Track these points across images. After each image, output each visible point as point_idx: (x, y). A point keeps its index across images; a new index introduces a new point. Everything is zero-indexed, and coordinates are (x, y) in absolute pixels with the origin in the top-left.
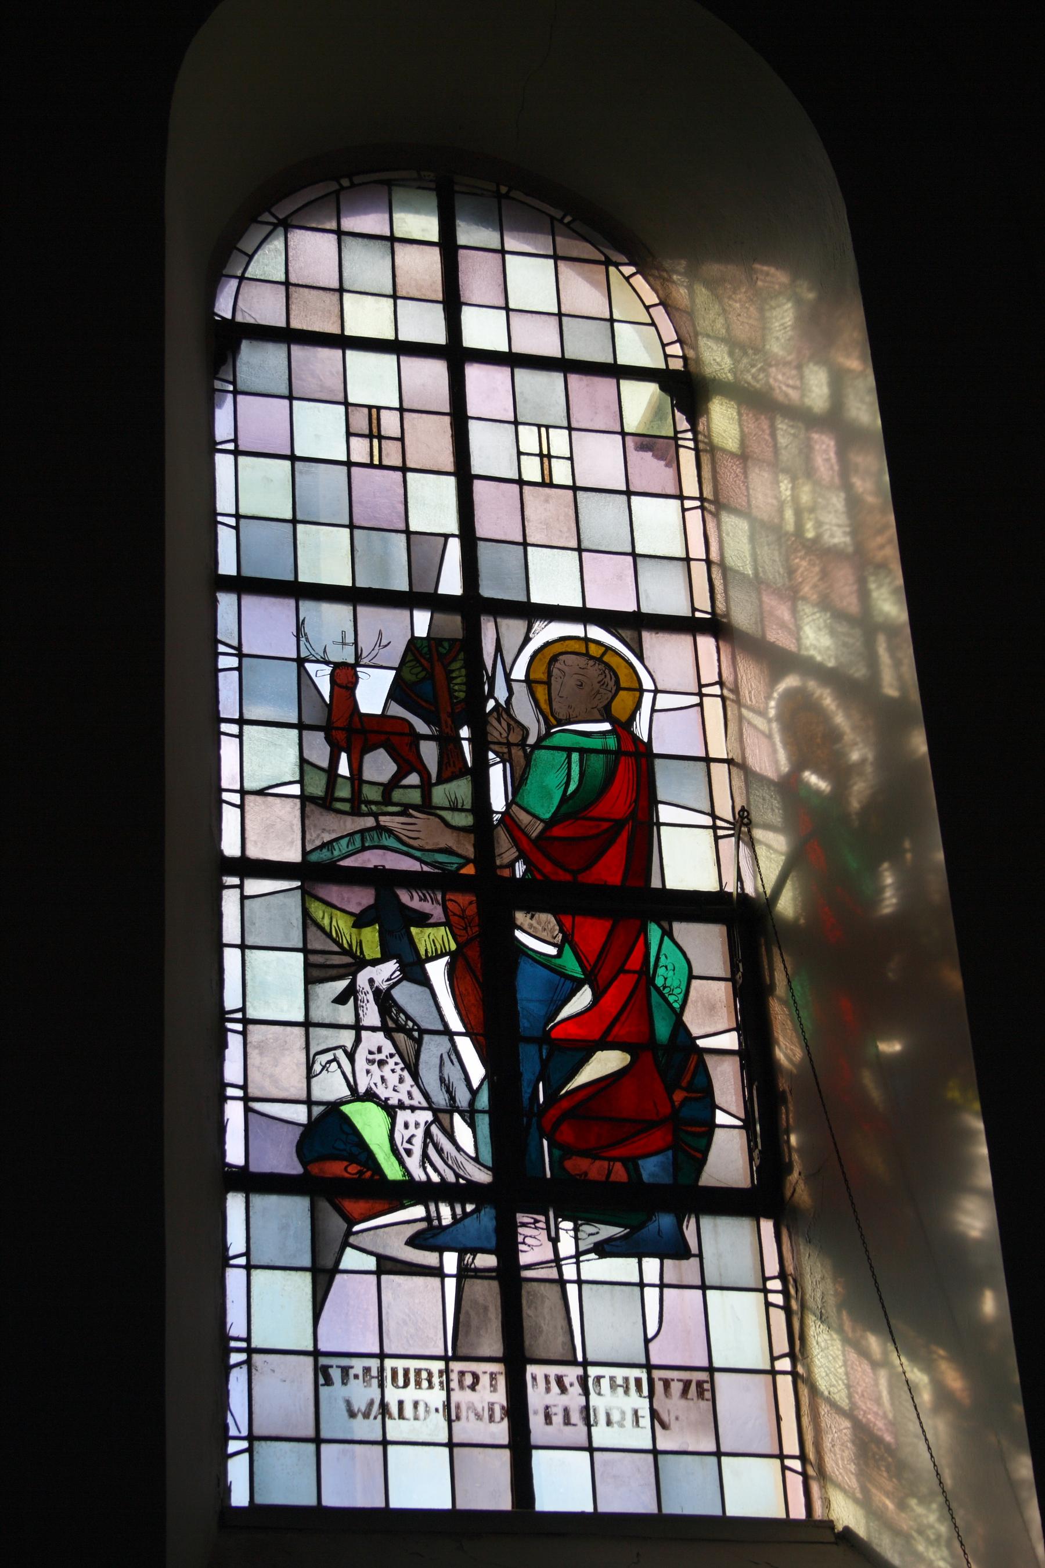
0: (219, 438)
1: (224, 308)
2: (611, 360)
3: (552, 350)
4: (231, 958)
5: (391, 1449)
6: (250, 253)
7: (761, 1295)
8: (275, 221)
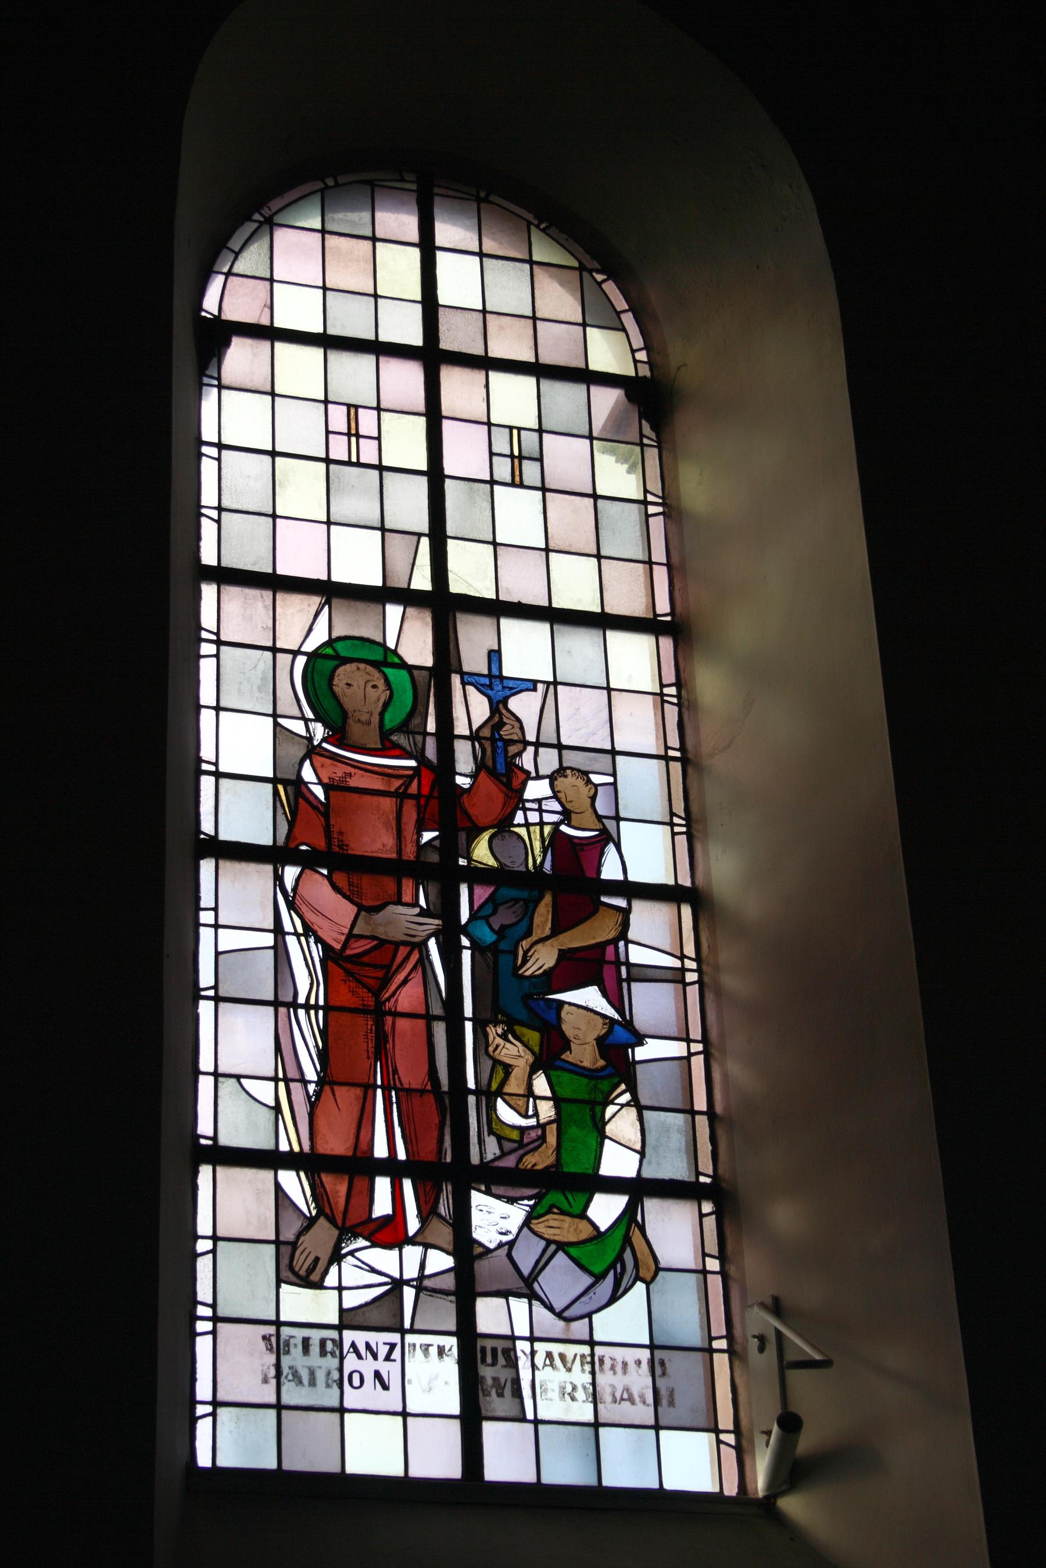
0: (202, 985)
1: (210, 304)
2: (582, 365)
3: (526, 355)
4: (207, 718)
5: (344, 1284)
6: (237, 250)
7: (713, 1435)
8: (262, 219)
